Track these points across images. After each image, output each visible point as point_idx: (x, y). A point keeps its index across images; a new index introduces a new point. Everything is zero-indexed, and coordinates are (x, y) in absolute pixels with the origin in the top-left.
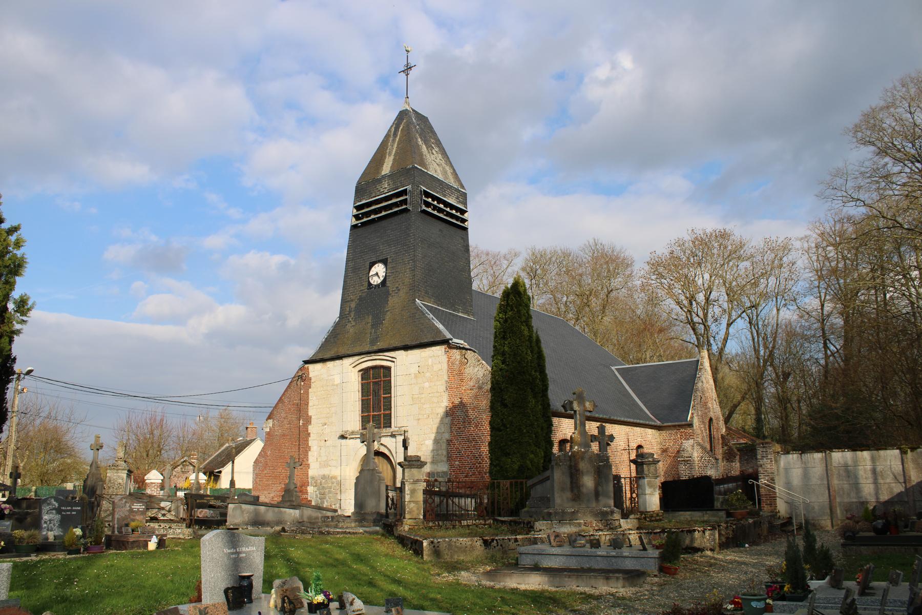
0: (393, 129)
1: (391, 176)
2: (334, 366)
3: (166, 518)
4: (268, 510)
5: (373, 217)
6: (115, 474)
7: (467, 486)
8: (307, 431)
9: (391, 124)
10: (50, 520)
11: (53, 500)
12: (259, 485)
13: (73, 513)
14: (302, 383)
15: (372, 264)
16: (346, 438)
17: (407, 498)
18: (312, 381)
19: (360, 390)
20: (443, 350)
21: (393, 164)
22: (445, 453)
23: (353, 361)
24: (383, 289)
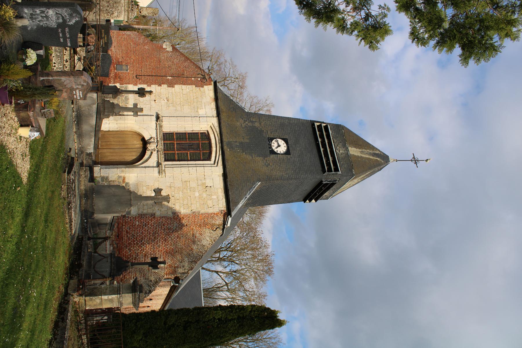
0: (377, 152)
1: (348, 155)
2: (212, 109)
3: (76, 62)
4: (92, 127)
5: (320, 140)
6: (123, 8)
7: (119, 233)
8: (163, 84)
9: (381, 150)
10: (47, 17)
11: (77, 19)
12: (122, 38)
13: (62, 40)
14: (199, 79)
15: (286, 141)
16: (157, 121)
17: (105, 297)
18: (201, 88)
19: (193, 132)
20: (223, 209)
21: (355, 156)
22: (145, 212)
23: (216, 127)
24: (268, 152)
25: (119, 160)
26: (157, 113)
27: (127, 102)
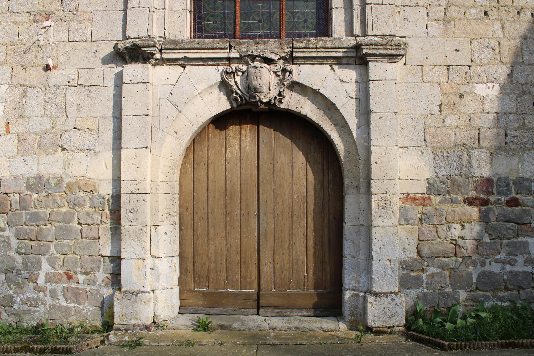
25: (310, 218)
26: (106, 61)
27: (53, 182)
